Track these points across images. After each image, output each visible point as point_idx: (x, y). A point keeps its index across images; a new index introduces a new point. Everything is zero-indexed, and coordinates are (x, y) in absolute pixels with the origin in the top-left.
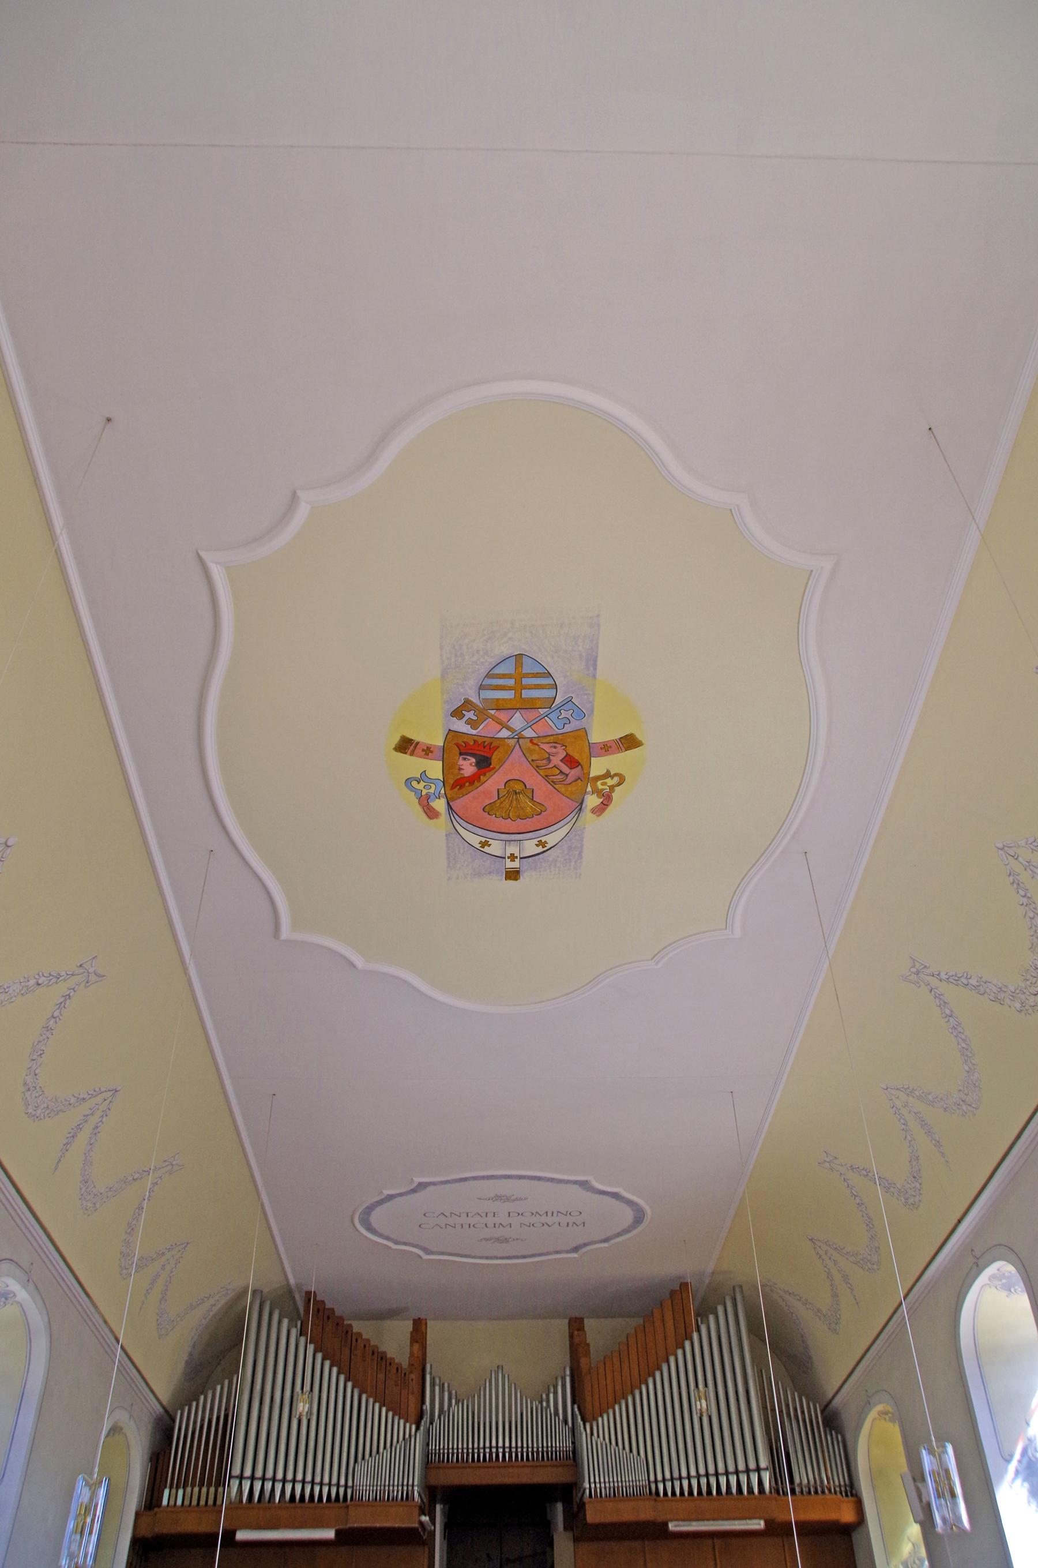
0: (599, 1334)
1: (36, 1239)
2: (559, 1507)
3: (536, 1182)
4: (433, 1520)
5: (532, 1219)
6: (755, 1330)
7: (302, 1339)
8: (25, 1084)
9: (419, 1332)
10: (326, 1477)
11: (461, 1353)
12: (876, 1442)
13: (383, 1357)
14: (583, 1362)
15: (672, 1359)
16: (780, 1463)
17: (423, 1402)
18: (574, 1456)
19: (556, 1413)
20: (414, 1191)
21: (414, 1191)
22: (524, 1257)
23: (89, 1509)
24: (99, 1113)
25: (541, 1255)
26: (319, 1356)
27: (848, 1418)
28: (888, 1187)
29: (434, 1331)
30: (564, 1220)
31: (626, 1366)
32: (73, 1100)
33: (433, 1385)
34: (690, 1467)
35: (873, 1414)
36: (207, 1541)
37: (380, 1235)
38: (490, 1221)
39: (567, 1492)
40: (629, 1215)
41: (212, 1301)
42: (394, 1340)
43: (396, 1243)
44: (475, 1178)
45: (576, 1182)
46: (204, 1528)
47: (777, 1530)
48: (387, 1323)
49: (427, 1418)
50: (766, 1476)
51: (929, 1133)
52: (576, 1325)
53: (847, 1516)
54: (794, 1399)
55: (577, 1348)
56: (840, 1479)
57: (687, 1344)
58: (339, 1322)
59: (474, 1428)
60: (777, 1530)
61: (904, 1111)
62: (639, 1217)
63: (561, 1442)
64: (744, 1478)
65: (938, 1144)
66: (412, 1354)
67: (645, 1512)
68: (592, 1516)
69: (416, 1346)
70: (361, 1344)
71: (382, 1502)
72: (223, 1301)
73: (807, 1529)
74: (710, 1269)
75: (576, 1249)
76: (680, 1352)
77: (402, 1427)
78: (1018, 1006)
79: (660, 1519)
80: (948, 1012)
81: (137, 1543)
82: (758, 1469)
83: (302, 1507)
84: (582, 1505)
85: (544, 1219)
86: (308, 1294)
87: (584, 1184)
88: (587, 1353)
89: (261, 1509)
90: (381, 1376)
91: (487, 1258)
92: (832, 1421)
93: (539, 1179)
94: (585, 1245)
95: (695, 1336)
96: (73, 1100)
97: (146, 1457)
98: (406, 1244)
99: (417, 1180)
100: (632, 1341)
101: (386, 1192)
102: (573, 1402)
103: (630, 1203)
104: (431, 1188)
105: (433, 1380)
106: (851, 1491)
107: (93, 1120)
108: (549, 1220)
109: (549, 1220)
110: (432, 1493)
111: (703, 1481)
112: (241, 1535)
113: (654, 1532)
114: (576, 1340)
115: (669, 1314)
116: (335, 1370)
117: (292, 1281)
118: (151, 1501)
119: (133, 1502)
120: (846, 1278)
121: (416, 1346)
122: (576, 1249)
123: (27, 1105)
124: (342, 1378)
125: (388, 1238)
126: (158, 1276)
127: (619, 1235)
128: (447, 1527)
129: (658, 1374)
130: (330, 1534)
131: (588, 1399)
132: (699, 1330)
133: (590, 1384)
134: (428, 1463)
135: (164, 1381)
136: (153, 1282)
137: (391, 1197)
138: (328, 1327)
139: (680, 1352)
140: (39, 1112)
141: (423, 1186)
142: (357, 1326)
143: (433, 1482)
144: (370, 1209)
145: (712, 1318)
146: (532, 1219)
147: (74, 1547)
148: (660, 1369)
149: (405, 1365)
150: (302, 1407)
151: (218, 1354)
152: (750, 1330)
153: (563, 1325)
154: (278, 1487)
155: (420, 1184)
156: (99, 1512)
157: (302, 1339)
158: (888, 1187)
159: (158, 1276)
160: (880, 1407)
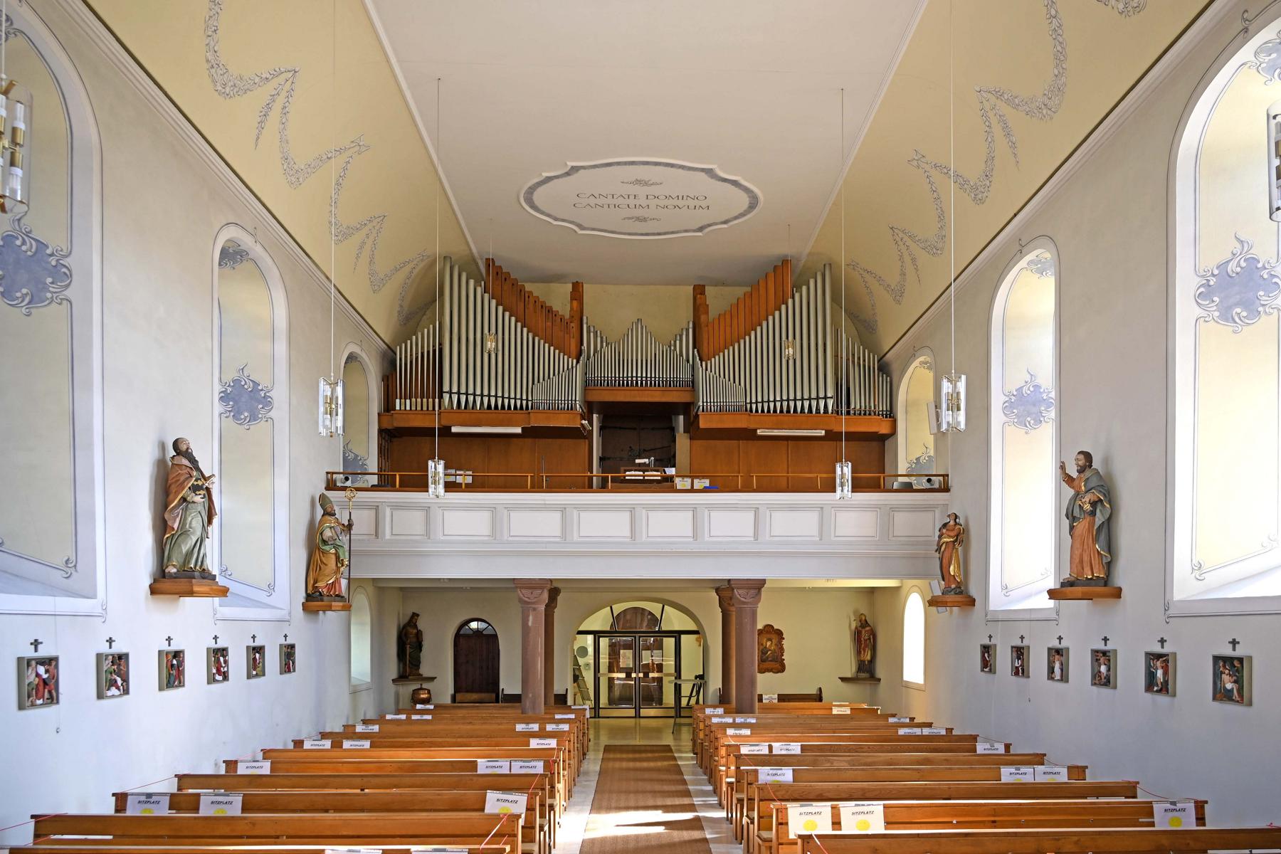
0: (717, 300)
1: (652, 780)
2: (681, 418)
3: (669, 169)
4: (591, 423)
5: (666, 202)
6: (836, 299)
7: (486, 296)
8: (208, 61)
9: (577, 292)
10: (513, 392)
11: (609, 311)
12: (914, 384)
13: (550, 310)
14: (703, 318)
15: (770, 318)
16: (843, 394)
17: (582, 344)
18: (692, 385)
19: (681, 355)
20: (567, 174)
21: (567, 174)
22: (659, 234)
23: (332, 400)
24: (284, 94)
25: (673, 233)
26: (500, 308)
27: (895, 368)
28: (962, 183)
29: (587, 289)
30: (692, 203)
31: (735, 322)
32: (257, 80)
33: (589, 332)
34: (776, 394)
35: (916, 363)
36: (429, 432)
37: (543, 213)
38: (632, 202)
39: (687, 408)
40: (744, 201)
41: (412, 265)
42: (559, 298)
43: (556, 219)
44: (618, 164)
45: (703, 170)
46: (427, 424)
47: (832, 436)
48: (554, 286)
49: (584, 355)
50: (830, 402)
51: (1008, 135)
52: (699, 290)
53: (884, 429)
54: (859, 350)
55: (699, 307)
56: (883, 407)
57: (783, 307)
58: (514, 283)
59: (620, 362)
60: (832, 436)
61: (991, 114)
62: (752, 206)
63: (685, 375)
64: (814, 403)
65: (1013, 145)
66: (572, 309)
67: (741, 422)
68: (703, 424)
69: (575, 303)
70: (532, 300)
71: (554, 409)
72: (421, 265)
73: (851, 436)
74: (807, 251)
75: (701, 229)
76: (777, 313)
77: (567, 362)
78: (1121, 6)
79: (752, 426)
80: (1053, 12)
81: (381, 431)
82: (825, 398)
83: (496, 412)
84: (697, 416)
85: (676, 202)
86: (488, 260)
87: (710, 172)
88: (707, 313)
89: (467, 412)
90: (549, 324)
91: (630, 234)
92: (884, 368)
93: (672, 166)
94: (709, 225)
95: (790, 301)
96: (257, 80)
97: (380, 379)
98: (563, 220)
99: (571, 164)
100: (734, 311)
101: (545, 174)
102: (694, 347)
103: (746, 190)
104: (582, 171)
105: (588, 328)
106: (891, 415)
107: (280, 101)
108: (680, 203)
109: (680, 203)
110: (590, 407)
111: (785, 404)
112: (454, 430)
113: (748, 435)
114: (698, 302)
115: (775, 282)
116: (513, 319)
117: (474, 250)
118: (388, 406)
119: (375, 407)
120: (914, 260)
121: (575, 303)
122: (701, 229)
123: (214, 82)
124: (519, 325)
125: (549, 215)
126: (364, 243)
127: (736, 218)
128: (601, 429)
129: (759, 329)
130: (518, 430)
131: (705, 344)
132: (793, 298)
133: (705, 335)
134: (587, 385)
135: (384, 325)
136: (361, 248)
137: (549, 179)
138: (502, 284)
139: (777, 313)
140: (228, 90)
141: (575, 169)
142: (529, 287)
143: (590, 399)
144: (532, 190)
145: (804, 288)
146: (666, 202)
147: (328, 423)
148: (761, 325)
149: (567, 316)
150: (490, 345)
151: (421, 307)
152: (833, 300)
153: (689, 290)
154: (478, 399)
155: (573, 168)
156: (340, 401)
157: (486, 296)
158: (962, 183)
159: (364, 243)
160: (922, 359)
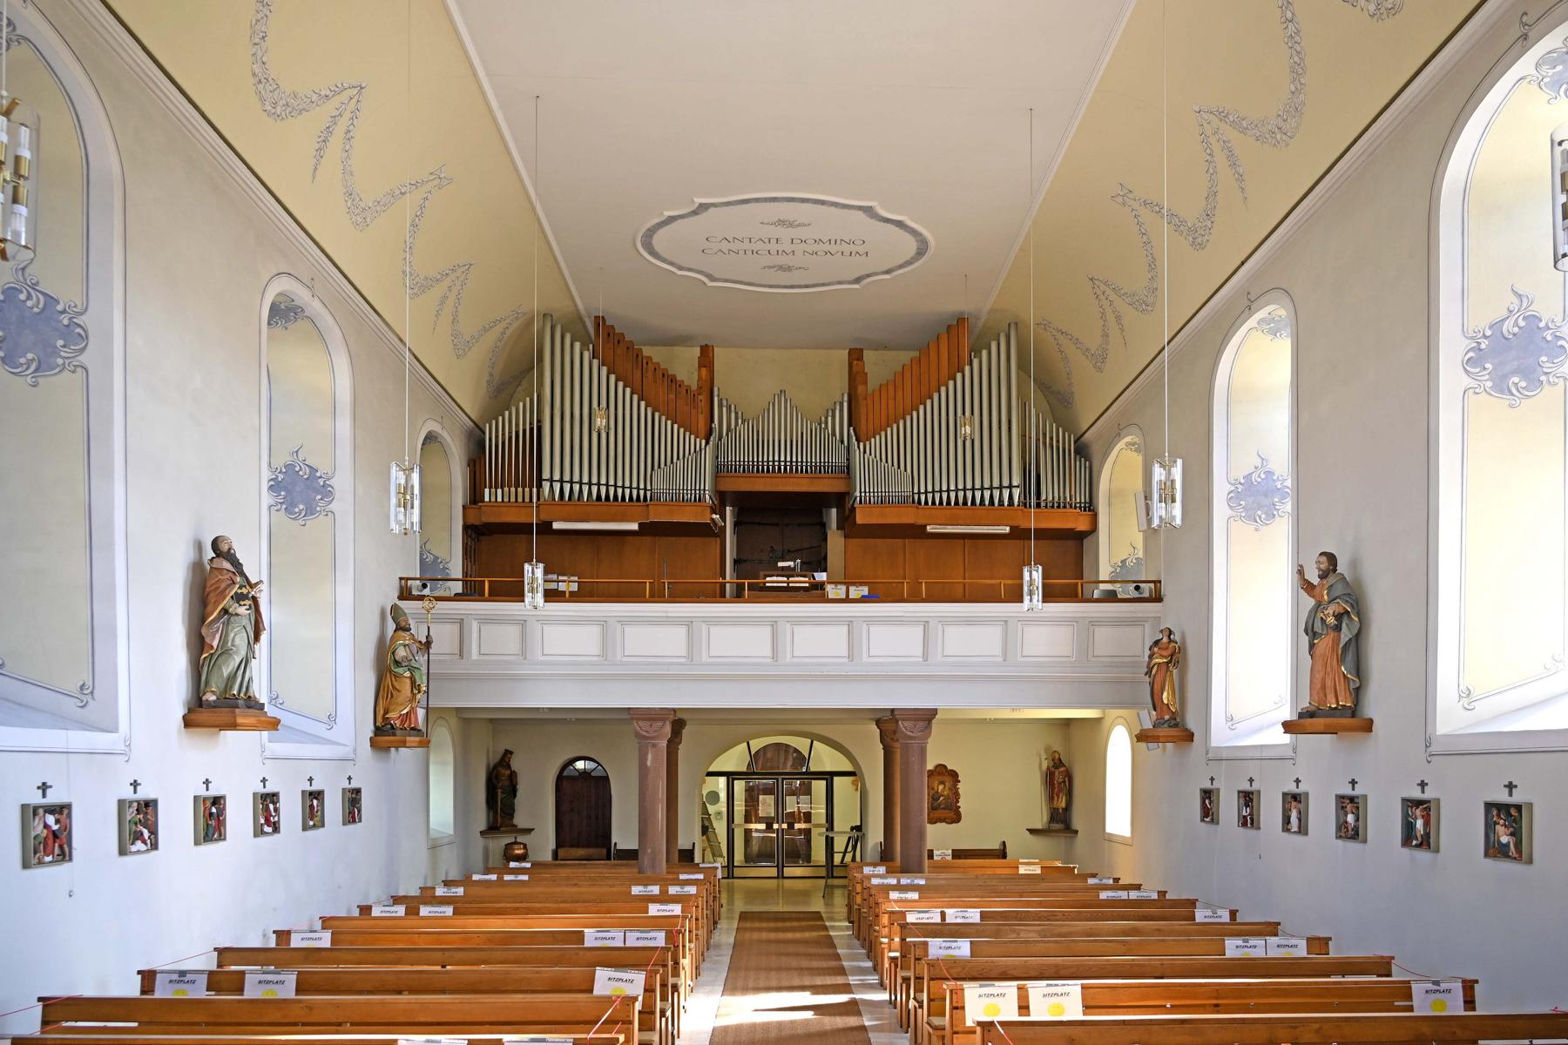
0: (878, 367)
2: (834, 511)
3: (819, 207)
4: (723, 518)
5: (816, 247)
6: (1023, 366)
7: (595, 362)
8: (254, 74)
9: (706, 358)
10: (628, 480)
11: (745, 380)
12: (1119, 470)
13: (673, 379)
14: (860, 389)
15: (943, 389)
16: (1031, 483)
17: (712, 421)
18: (847, 471)
19: (834, 434)
20: (695, 213)
21: (695, 213)
22: (807, 286)
23: (406, 489)
24: (347, 115)
25: (823, 285)
26: (613, 377)
27: (1096, 450)
28: (1177, 223)
29: (719, 353)
30: (847, 248)
31: (899, 394)
32: (315, 98)
33: (720, 406)
34: (949, 482)
35: (1121, 444)
36: (525, 529)
37: (664, 261)
38: (773, 247)
39: (841, 500)
40: (911, 245)
41: (504, 325)
42: (684, 365)
43: (681, 268)
44: (757, 200)
45: (860, 208)
46: (522, 519)
47: (1019, 534)
48: (678, 350)
49: (715, 434)
50: (1016, 492)
51: (1234, 165)
52: (856, 355)
53: (1082, 525)
54: (1052, 429)
55: (855, 376)
56: (1081, 498)
57: (959, 376)
58: (630, 347)
59: (759, 443)
60: (1019, 534)
61: (1213, 140)
62: (921, 252)
63: (839, 459)
64: (996, 493)
65: (1240, 178)
66: (700, 378)
67: (907, 517)
68: (861, 518)
69: (704, 371)
70: (651, 367)
71: (678, 500)
72: (516, 325)
73: (1042, 534)
74: (988, 307)
75: (858, 280)
76: (951, 383)
77: (694, 443)
78: (1372, 7)
79: (921, 522)
80: (1289, 15)
81: (466, 528)
82: (1010, 487)
83: (608, 504)
84: (853, 509)
85: (827, 247)
86: (597, 318)
87: (869, 211)
88: (865, 383)
89: (571, 505)
90: (672, 396)
91: (771, 286)
92: (1082, 451)
93: (823, 203)
94: (868, 276)
95: (967, 368)
96: (315, 98)
97: (465, 464)
98: (690, 270)
99: (698, 200)
101: (667, 213)
102: (850, 425)
103: (913, 232)
104: (712, 210)
105: (720, 401)
106: (1090, 507)
107: (343, 123)
108: (833, 248)
109: (833, 248)
110: (722, 498)
111: (961, 494)
112: (556, 526)
113: (916, 532)
114: (855, 369)
115: (948, 345)
116: (628, 390)
117: (581, 306)
118: (475, 497)
119: (459, 498)
120: (1118, 318)
121: (704, 371)
122: (858, 280)
123: (262, 100)
124: (635, 397)
125: (671, 264)
126: (445, 297)
127: (901, 267)
128: (736, 524)
129: (929, 402)
130: (634, 526)
131: (863, 421)
132: (971, 364)
133: (863, 409)
134: (718, 471)
135: (470, 398)
136: (442, 303)
137: (672, 219)
138: (615, 347)
139: (951, 383)
140: (278, 110)
141: (704, 207)
142: (647, 351)
143: (722, 488)
144: (651, 232)
145: (984, 353)
146: (816, 247)
147: (401, 517)
148: (931, 398)
149: (694, 387)
150: (600, 422)
151: (515, 375)
152: (1019, 367)
153: (844, 354)
154: (586, 489)
155: (701, 205)
156: (417, 491)
157: (595, 362)
158: (1177, 223)
159: (445, 297)
160: (1128, 439)
